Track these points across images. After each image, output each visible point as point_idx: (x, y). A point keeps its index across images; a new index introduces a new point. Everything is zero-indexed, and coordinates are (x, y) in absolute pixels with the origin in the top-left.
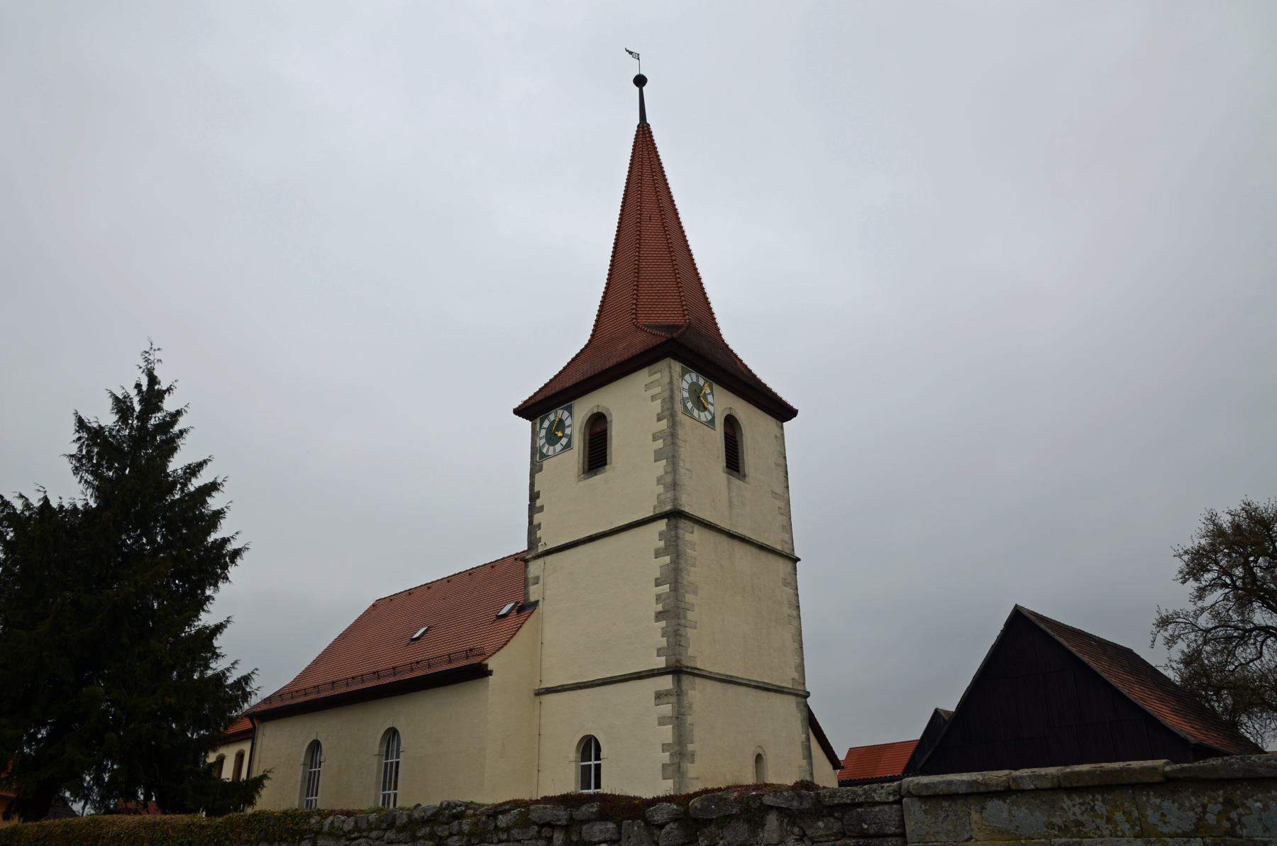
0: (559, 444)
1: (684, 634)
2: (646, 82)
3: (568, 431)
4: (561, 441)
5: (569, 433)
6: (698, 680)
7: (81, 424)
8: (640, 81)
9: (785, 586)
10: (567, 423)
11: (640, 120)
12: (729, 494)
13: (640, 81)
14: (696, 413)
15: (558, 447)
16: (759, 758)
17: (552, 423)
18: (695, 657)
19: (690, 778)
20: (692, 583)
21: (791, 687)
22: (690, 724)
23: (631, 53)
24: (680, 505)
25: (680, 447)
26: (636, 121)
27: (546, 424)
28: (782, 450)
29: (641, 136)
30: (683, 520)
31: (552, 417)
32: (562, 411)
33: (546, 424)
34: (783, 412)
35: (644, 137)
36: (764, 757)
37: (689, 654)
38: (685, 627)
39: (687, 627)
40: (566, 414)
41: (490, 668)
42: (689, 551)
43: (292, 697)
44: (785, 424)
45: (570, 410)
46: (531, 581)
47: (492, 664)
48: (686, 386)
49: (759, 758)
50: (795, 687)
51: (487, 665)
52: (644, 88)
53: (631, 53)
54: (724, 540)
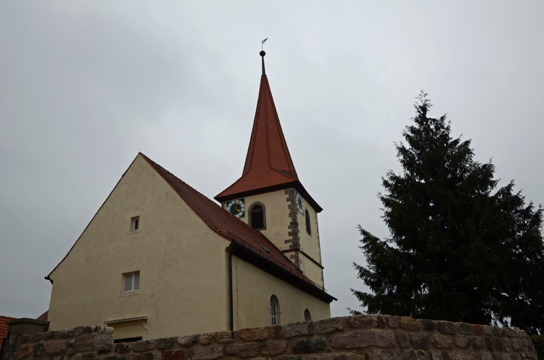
2: (260, 53)
3: (242, 210)
4: (239, 214)
5: (244, 211)
7: (361, 241)
8: (263, 54)
10: (242, 206)
11: (263, 73)
13: (263, 54)
17: (235, 204)
23: (265, 40)
27: (230, 205)
28: (316, 221)
29: (264, 79)
31: (233, 202)
32: (239, 200)
33: (230, 205)
34: (318, 209)
35: (264, 80)
40: (241, 202)
43: (212, 349)
44: (318, 213)
45: (243, 201)
47: (48, 320)
52: (264, 57)
53: (265, 40)
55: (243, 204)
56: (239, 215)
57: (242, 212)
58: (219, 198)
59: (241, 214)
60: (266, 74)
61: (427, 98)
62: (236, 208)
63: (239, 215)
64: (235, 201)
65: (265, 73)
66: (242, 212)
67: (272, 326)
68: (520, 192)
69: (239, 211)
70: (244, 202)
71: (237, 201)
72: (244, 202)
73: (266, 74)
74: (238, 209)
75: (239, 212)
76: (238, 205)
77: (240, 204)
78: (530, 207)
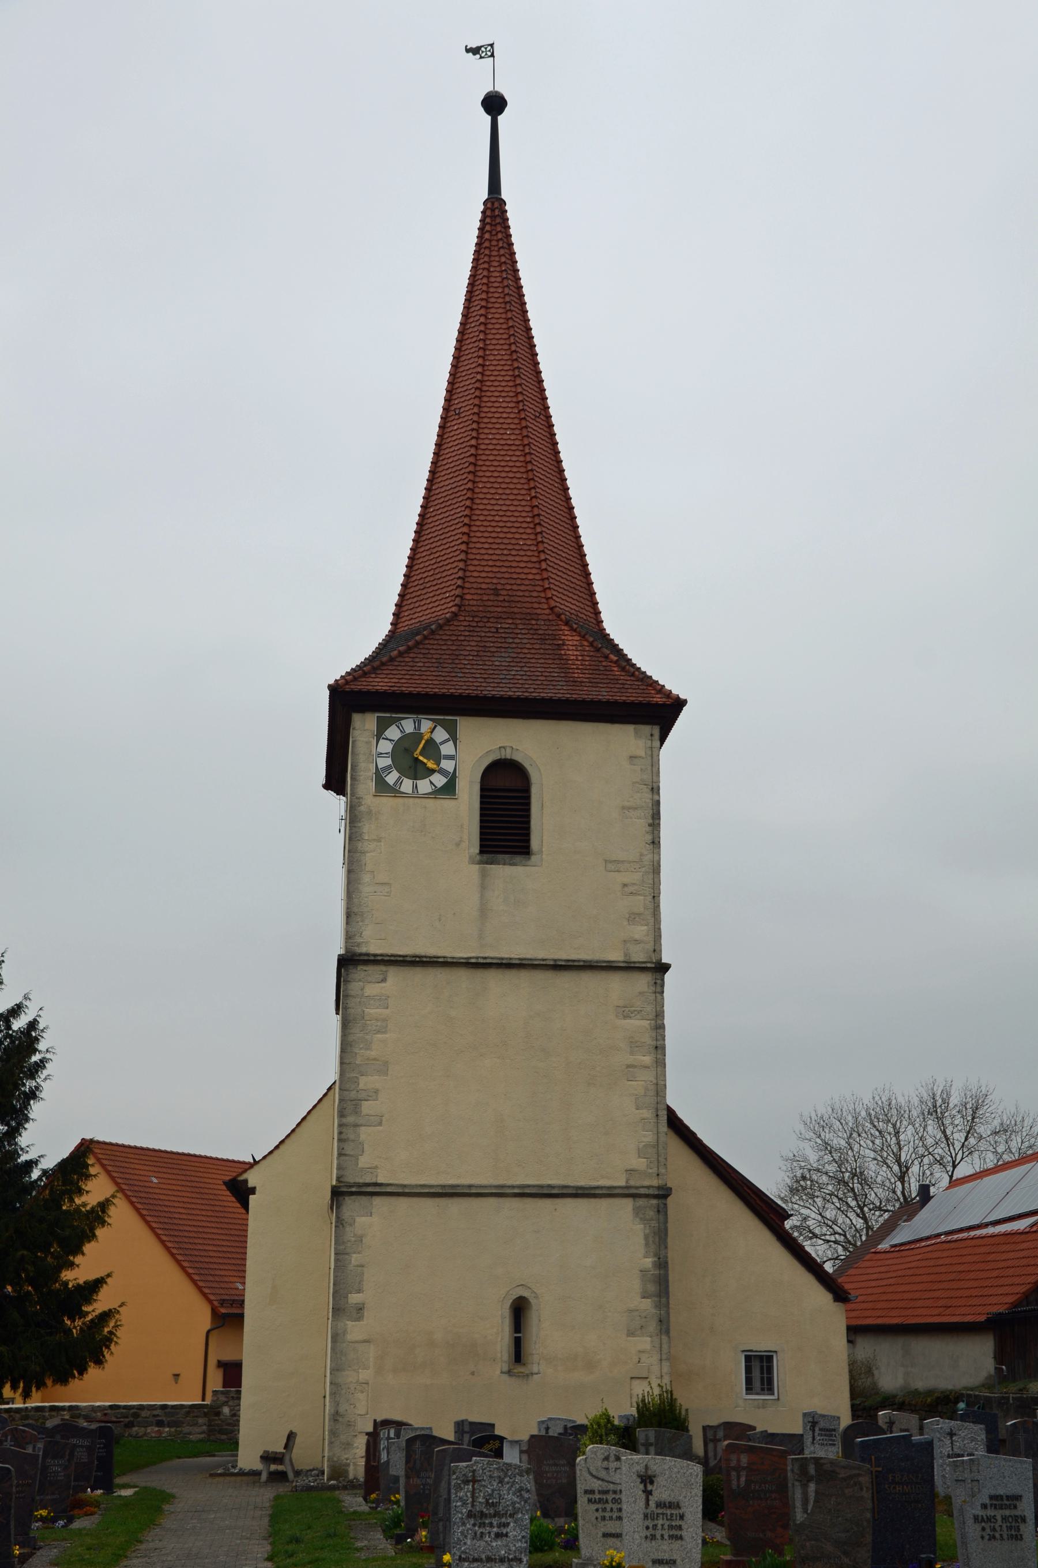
0: (428, 779)
1: (352, 1137)
6: (377, 1201)
8: (494, 104)
9: (625, 1017)
10: (447, 749)
12: (482, 896)
13: (494, 104)
14: (407, 785)
15: (424, 786)
16: (519, 1310)
17: (417, 736)
18: (376, 1167)
19: (349, 1342)
20: (375, 1059)
21: (622, 1183)
22: (358, 1266)
24: (359, 945)
25: (364, 853)
26: (483, 193)
30: (360, 967)
33: (393, 733)
36: (533, 1301)
37: (360, 1165)
38: (356, 1126)
39: (361, 1125)
41: (250, 1184)
42: (372, 1011)
46: (627, 958)
48: (386, 746)
49: (519, 1310)
50: (632, 1183)
51: (246, 1181)
52: (499, 118)
54: (463, 977)
55: (451, 742)
56: (431, 782)
57: (443, 772)
58: (352, 692)
59: (439, 780)
60: (504, 196)
61: (27, 1003)
62: (421, 754)
63: (431, 782)
64: (418, 725)
65: (498, 191)
66: (443, 772)
67: (518, 1463)
68: (32, 1145)
69: (431, 765)
70: (454, 738)
71: (426, 725)
72: (454, 738)
73: (504, 195)
74: (428, 759)
75: (433, 771)
76: (427, 741)
77: (438, 741)
78: (95, 1286)
